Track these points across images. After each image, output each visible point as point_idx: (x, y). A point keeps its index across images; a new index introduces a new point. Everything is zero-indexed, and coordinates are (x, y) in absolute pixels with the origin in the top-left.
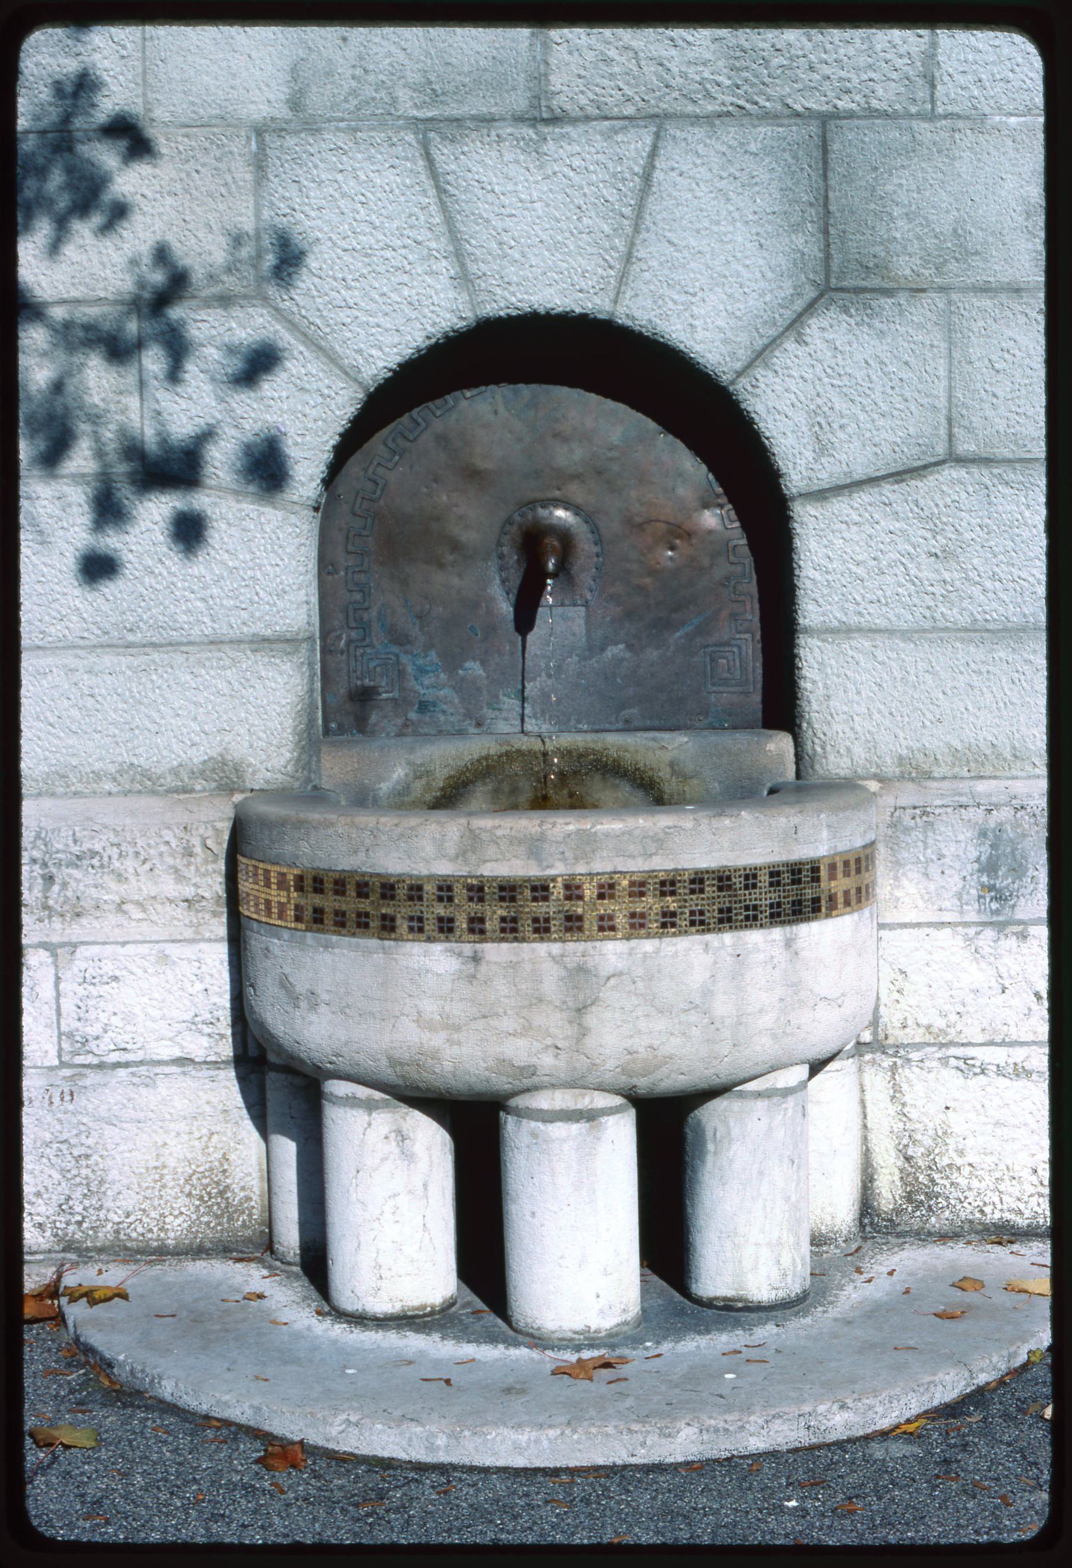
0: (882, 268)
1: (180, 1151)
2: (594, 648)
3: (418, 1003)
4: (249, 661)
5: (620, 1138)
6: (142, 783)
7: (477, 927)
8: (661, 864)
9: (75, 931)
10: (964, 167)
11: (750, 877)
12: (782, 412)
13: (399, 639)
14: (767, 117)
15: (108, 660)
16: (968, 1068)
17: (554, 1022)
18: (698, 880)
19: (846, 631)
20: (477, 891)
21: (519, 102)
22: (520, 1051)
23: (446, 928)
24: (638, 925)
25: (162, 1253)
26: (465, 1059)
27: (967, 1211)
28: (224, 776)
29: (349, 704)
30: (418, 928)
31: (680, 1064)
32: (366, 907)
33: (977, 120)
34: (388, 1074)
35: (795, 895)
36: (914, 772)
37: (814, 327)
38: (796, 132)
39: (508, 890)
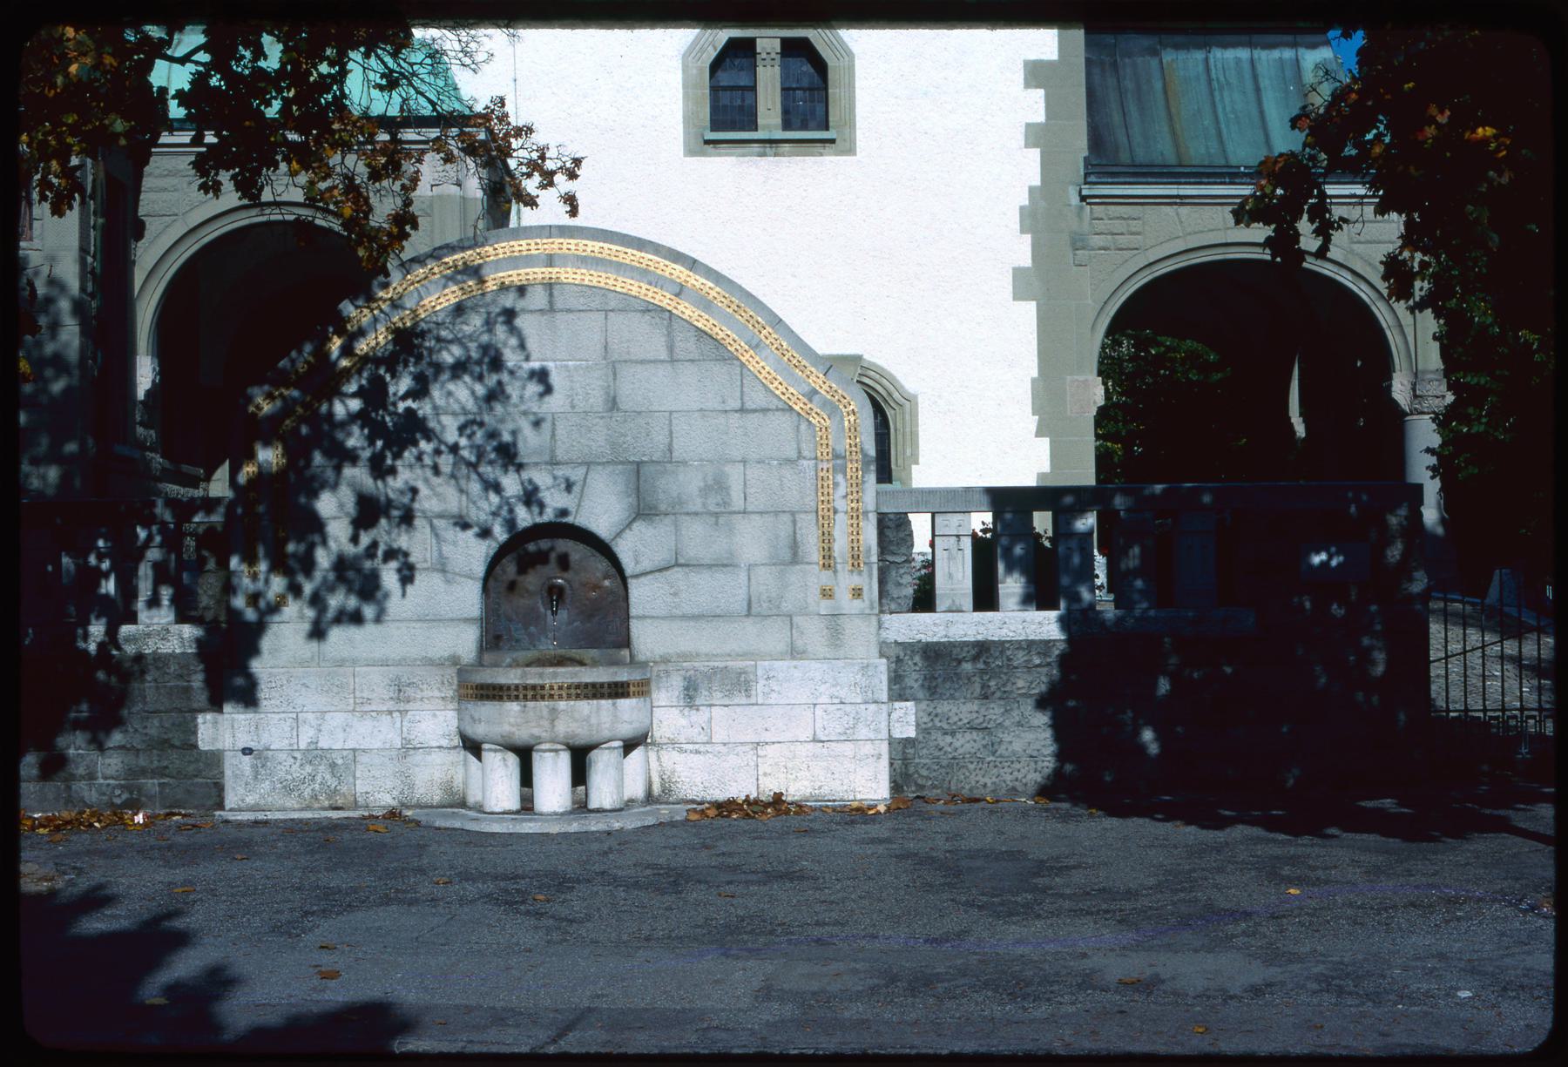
0: (655, 508)
1: (438, 776)
2: (570, 623)
3: (510, 719)
4: (463, 626)
5: (565, 759)
6: (430, 662)
7: (525, 698)
8: (576, 680)
9: (407, 707)
10: (681, 477)
11: (602, 685)
12: (625, 551)
13: (510, 620)
14: (622, 463)
15: (419, 625)
16: (681, 751)
17: (546, 723)
18: (586, 685)
19: (644, 617)
20: (525, 688)
21: (547, 458)
22: (536, 732)
23: (517, 698)
24: (569, 697)
25: (432, 807)
26: (522, 735)
27: (681, 796)
28: (454, 660)
29: (494, 638)
30: (509, 698)
31: (583, 735)
32: (494, 693)
33: (684, 463)
34: (500, 740)
35: (617, 691)
36: (665, 660)
37: (635, 526)
38: (630, 467)
39: (534, 687)
